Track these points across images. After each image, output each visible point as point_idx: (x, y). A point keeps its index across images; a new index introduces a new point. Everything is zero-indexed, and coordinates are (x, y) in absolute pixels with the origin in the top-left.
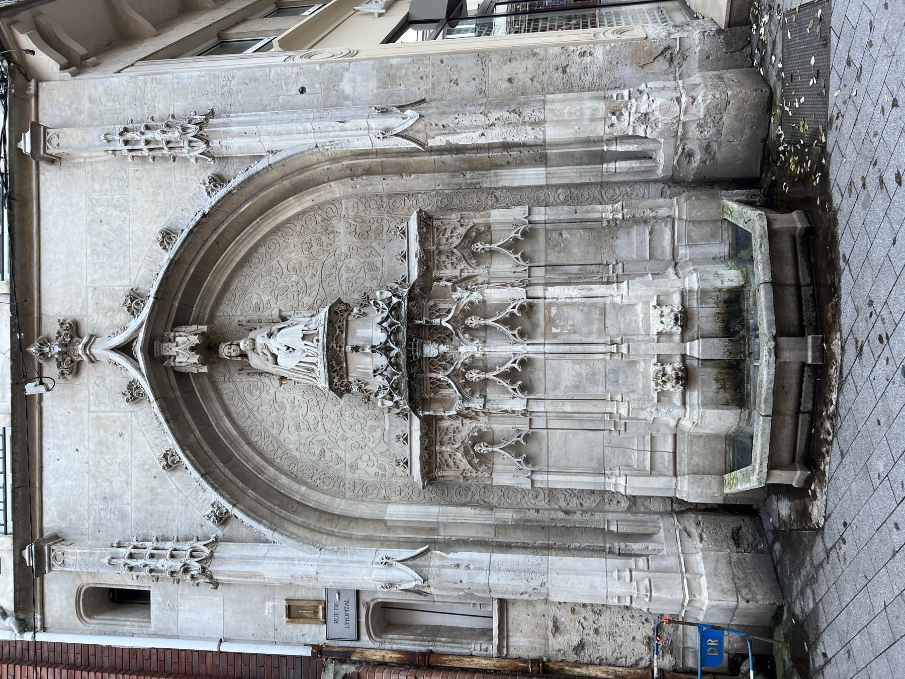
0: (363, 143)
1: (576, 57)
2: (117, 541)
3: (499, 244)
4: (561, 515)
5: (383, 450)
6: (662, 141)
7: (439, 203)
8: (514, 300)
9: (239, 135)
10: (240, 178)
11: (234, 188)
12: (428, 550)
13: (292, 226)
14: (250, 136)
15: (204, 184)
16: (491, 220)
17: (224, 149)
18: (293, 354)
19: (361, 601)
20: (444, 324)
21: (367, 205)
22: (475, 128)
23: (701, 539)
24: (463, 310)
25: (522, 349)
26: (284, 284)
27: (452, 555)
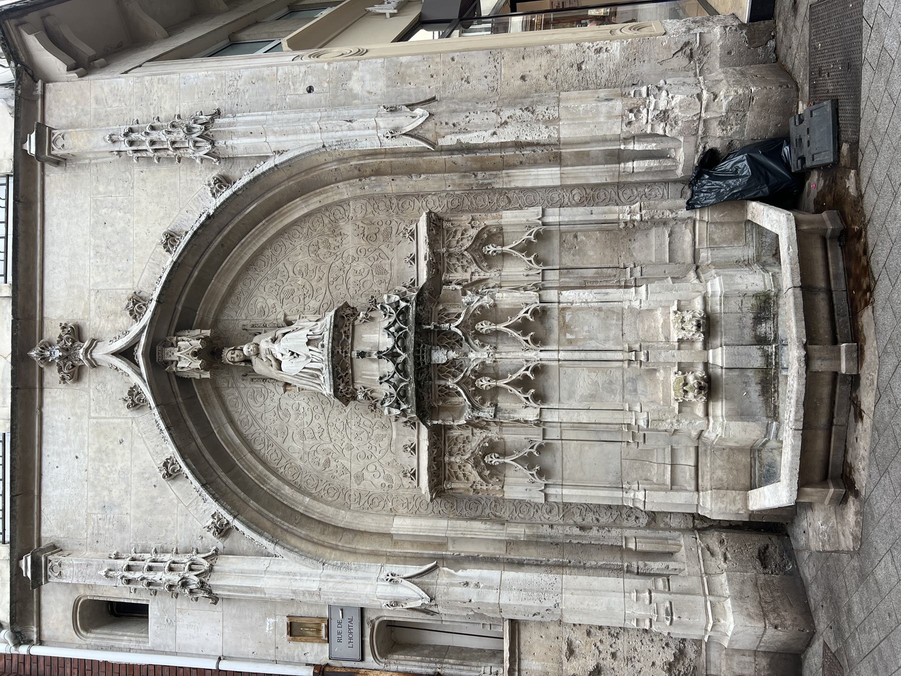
1: (592, 54)
2: (115, 552)
3: (511, 246)
4: (576, 531)
5: (390, 460)
6: (682, 139)
7: (450, 205)
8: (527, 304)
12: (435, 567)
13: (299, 229)
14: (256, 137)
15: (209, 185)
16: (503, 221)
17: (230, 150)
18: (297, 360)
20: (453, 329)
21: (376, 206)
23: (726, 559)
24: (473, 315)
25: (535, 355)
26: (290, 287)
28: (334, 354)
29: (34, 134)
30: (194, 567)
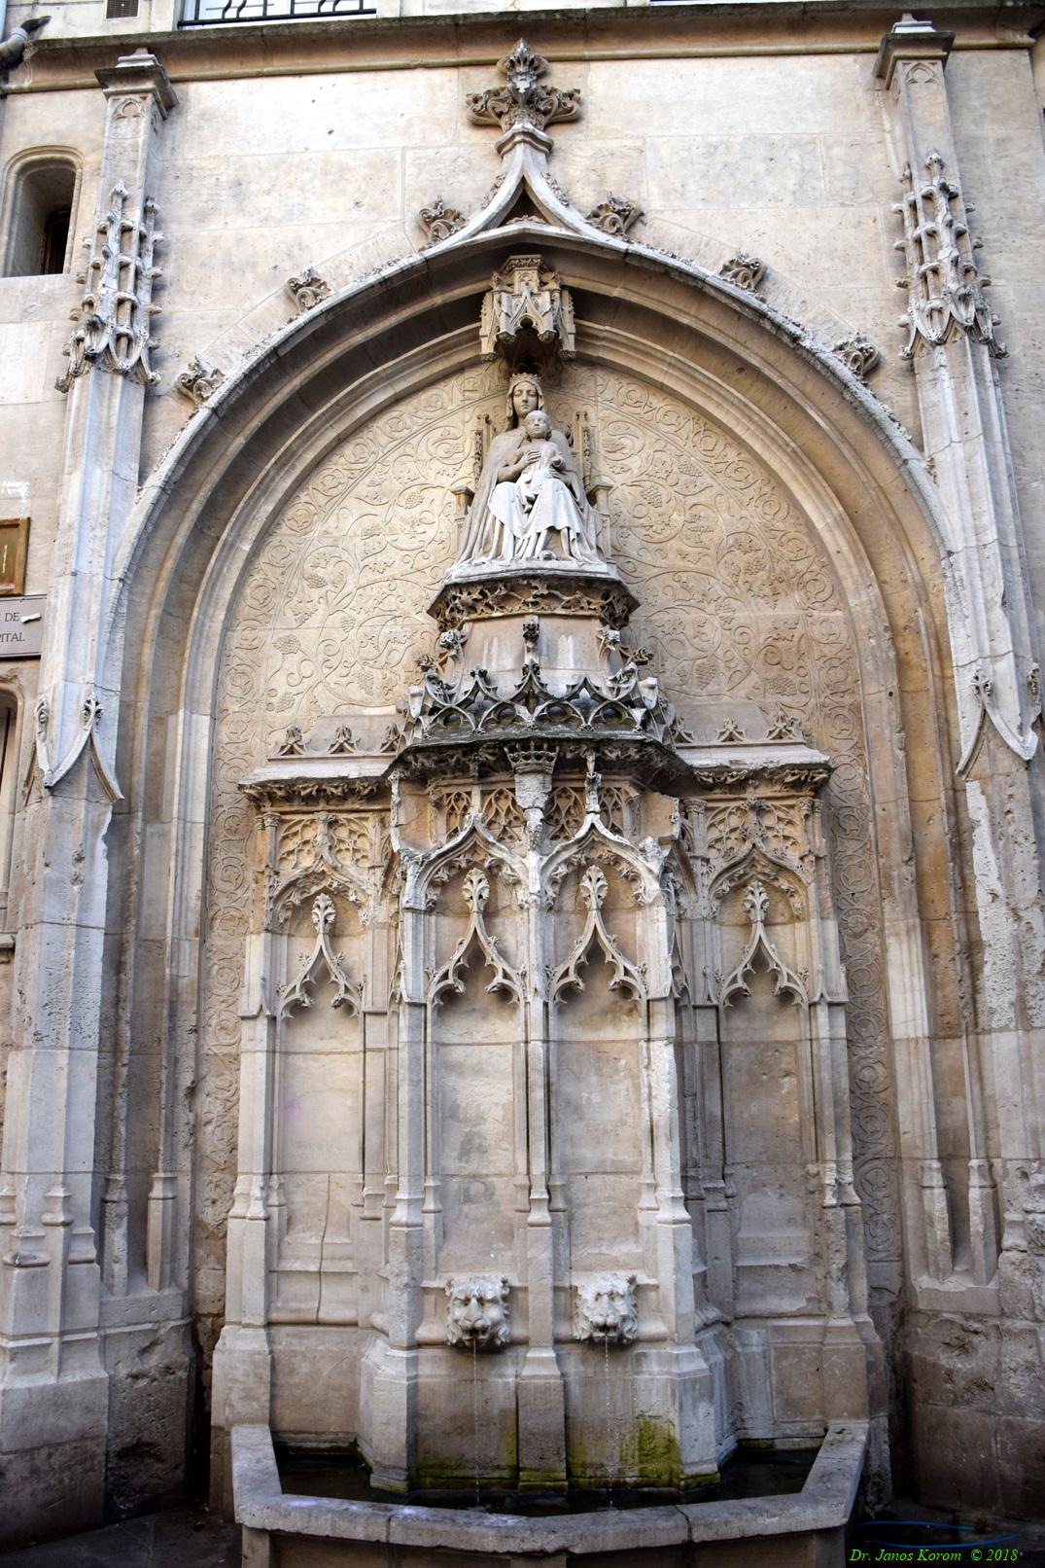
0: (962, 646)
2: (157, 207)
4: (186, 1079)
5: (322, 703)
6: (992, 1286)
7: (845, 812)
8: (643, 973)
9: (960, 403)
10: (876, 407)
11: (853, 394)
13: (783, 514)
14: (960, 422)
15: (859, 340)
17: (930, 375)
19: (19, 665)
20: (589, 819)
21: (836, 663)
22: (1006, 878)
23: (136, 1377)
24: (618, 860)
26: (665, 498)
27: (101, 847)
28: (530, 578)
29: (929, 30)
30: (124, 342)
